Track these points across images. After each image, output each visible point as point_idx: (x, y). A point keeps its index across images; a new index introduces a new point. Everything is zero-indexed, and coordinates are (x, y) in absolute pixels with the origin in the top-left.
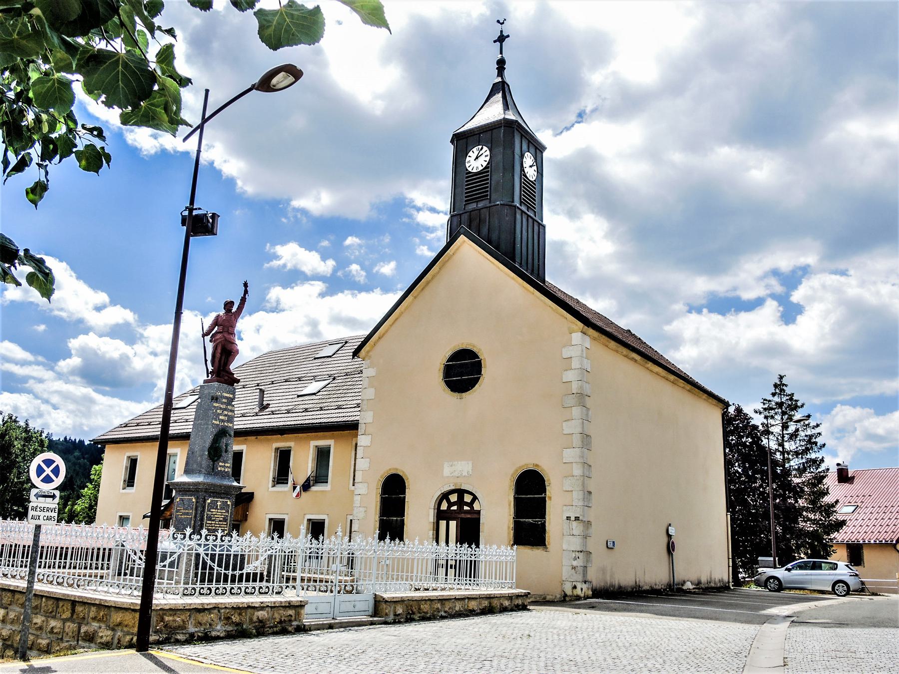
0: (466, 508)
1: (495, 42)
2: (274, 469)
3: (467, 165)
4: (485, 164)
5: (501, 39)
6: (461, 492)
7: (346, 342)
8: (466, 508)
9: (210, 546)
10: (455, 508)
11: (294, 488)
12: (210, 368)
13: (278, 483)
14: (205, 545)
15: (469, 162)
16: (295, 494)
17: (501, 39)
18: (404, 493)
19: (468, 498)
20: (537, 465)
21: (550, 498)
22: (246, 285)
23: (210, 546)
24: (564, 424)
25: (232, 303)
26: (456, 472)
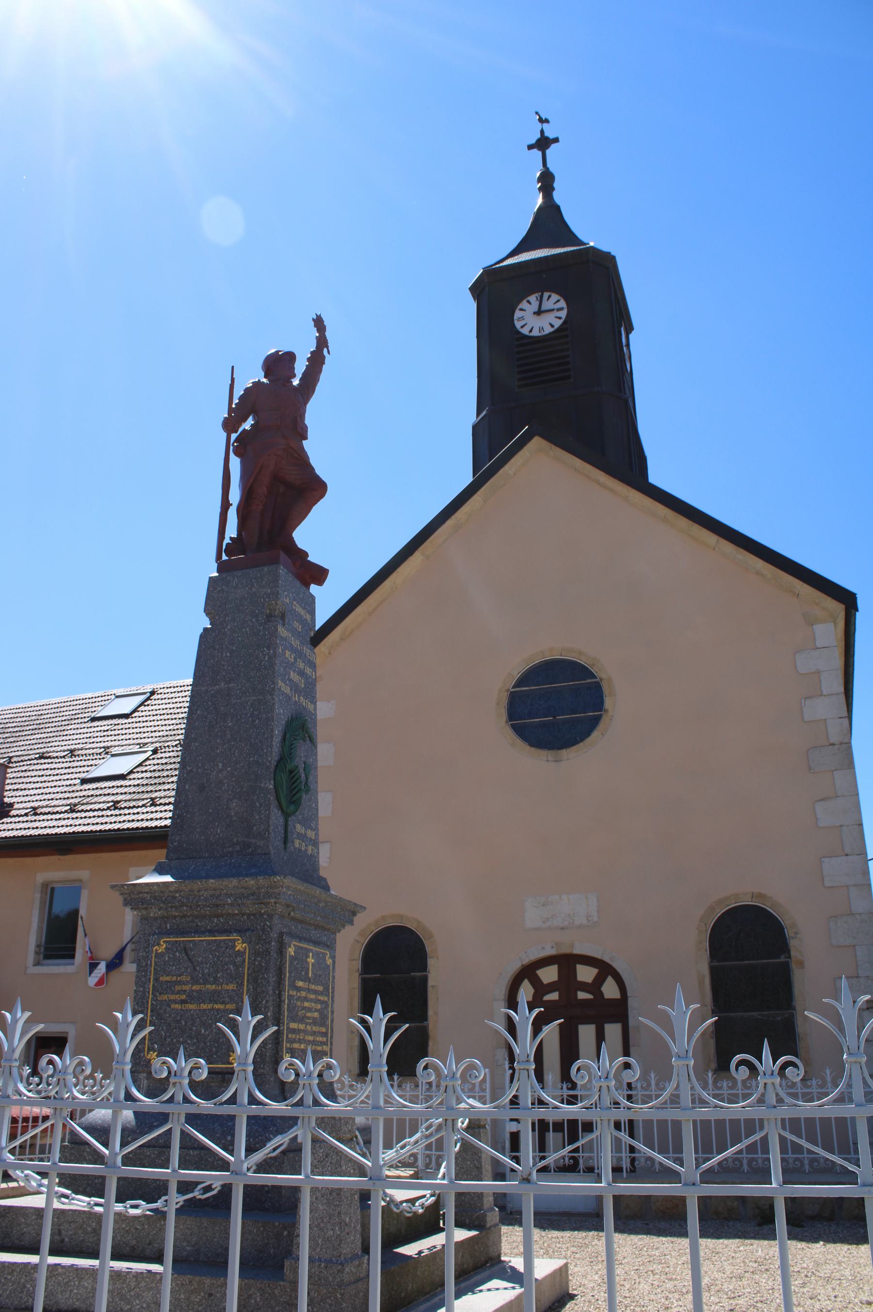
0: (582, 995)
1: (530, 147)
2: (40, 928)
3: (518, 324)
4: (548, 330)
5: (543, 143)
6: (567, 962)
7: (153, 693)
8: (582, 995)
9: (177, 1126)
10: (554, 996)
11: (93, 966)
12: (232, 531)
13: (47, 957)
14: (262, 1129)
15: (522, 318)
16: (92, 980)
17: (543, 143)
18: (424, 967)
19: (586, 974)
20: (761, 896)
21: (801, 964)
22: (319, 323)
23: (177, 1126)
24: (819, 807)
25: (290, 357)
26: (562, 917)
